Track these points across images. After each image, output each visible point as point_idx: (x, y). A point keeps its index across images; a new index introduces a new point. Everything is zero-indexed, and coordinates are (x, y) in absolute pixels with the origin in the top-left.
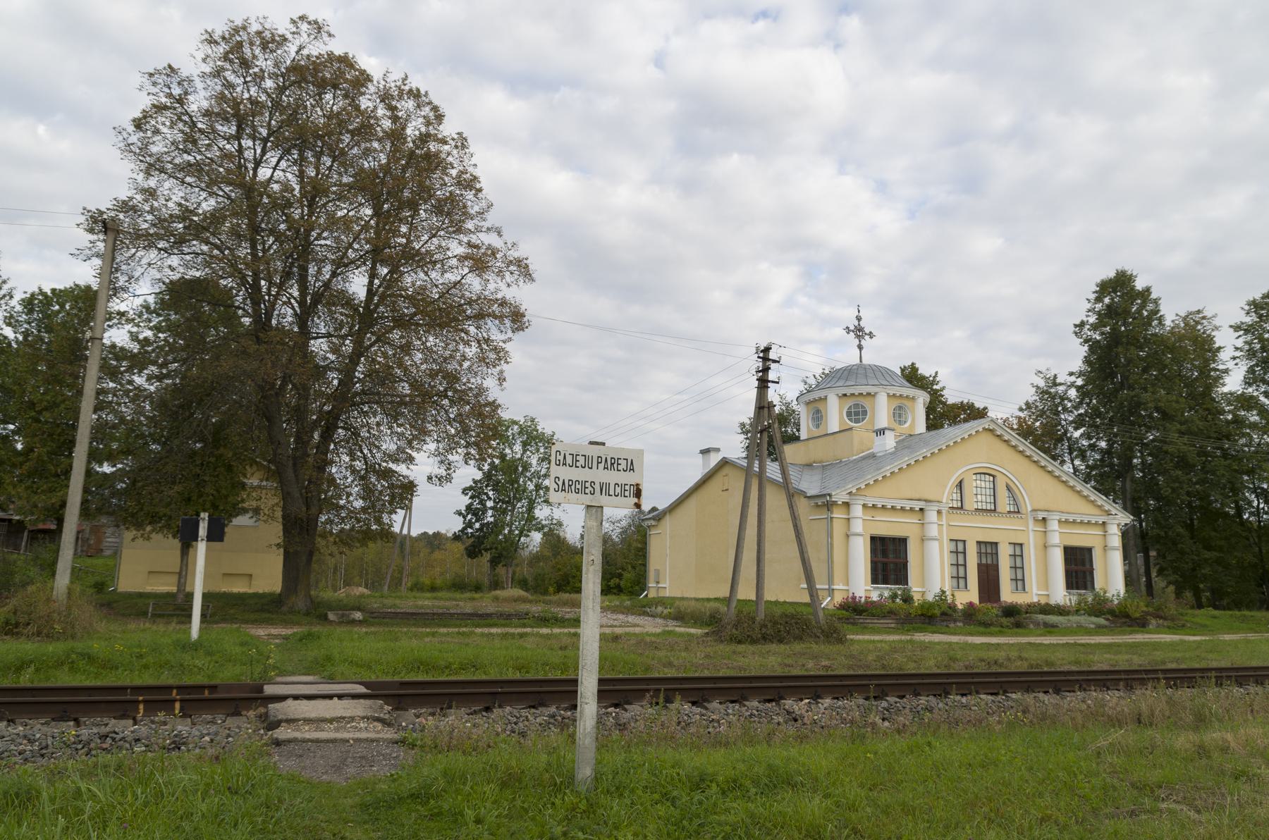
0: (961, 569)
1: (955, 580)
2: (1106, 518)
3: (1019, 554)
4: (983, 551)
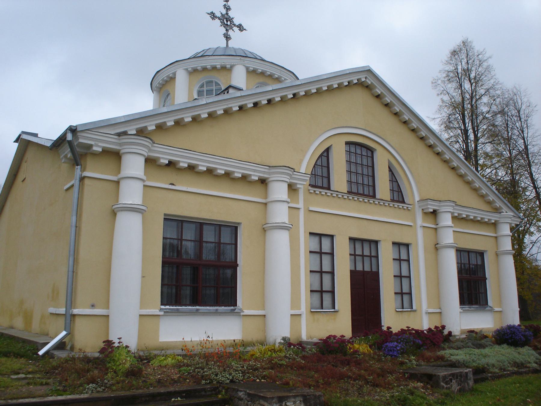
1: (317, 296)
4: (359, 252)
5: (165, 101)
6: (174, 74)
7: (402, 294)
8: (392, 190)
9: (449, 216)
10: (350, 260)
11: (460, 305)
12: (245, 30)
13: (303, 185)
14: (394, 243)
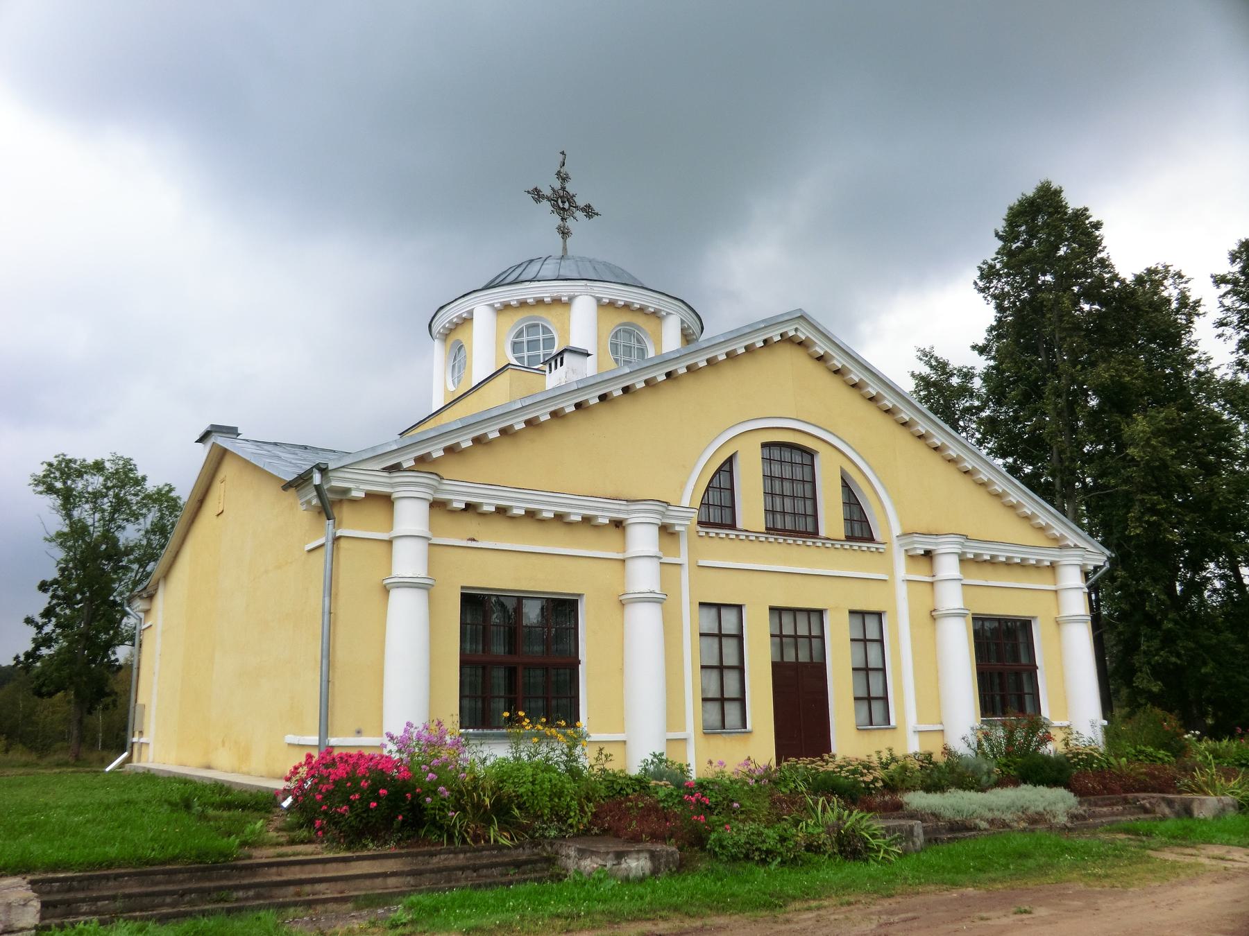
0: (731, 679)
1: (714, 708)
2: (1056, 552)
3: (876, 636)
5: (455, 359)
6: (471, 312)
7: (869, 699)
8: (849, 520)
9: (954, 560)
10: (773, 644)
11: (982, 717)
12: (597, 214)
13: (686, 521)
14: (852, 612)
